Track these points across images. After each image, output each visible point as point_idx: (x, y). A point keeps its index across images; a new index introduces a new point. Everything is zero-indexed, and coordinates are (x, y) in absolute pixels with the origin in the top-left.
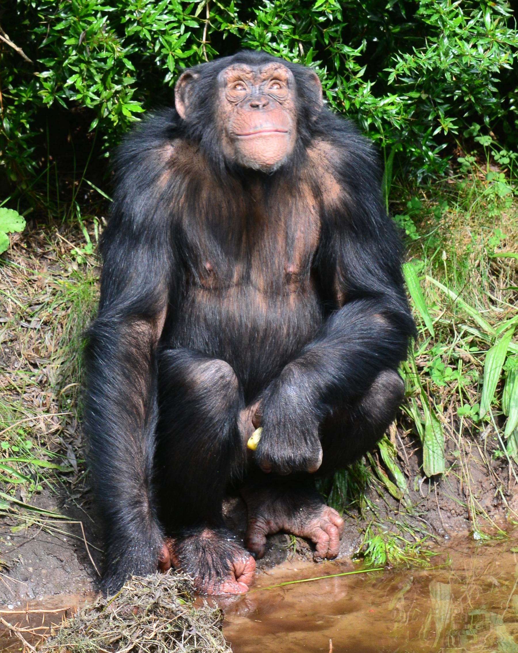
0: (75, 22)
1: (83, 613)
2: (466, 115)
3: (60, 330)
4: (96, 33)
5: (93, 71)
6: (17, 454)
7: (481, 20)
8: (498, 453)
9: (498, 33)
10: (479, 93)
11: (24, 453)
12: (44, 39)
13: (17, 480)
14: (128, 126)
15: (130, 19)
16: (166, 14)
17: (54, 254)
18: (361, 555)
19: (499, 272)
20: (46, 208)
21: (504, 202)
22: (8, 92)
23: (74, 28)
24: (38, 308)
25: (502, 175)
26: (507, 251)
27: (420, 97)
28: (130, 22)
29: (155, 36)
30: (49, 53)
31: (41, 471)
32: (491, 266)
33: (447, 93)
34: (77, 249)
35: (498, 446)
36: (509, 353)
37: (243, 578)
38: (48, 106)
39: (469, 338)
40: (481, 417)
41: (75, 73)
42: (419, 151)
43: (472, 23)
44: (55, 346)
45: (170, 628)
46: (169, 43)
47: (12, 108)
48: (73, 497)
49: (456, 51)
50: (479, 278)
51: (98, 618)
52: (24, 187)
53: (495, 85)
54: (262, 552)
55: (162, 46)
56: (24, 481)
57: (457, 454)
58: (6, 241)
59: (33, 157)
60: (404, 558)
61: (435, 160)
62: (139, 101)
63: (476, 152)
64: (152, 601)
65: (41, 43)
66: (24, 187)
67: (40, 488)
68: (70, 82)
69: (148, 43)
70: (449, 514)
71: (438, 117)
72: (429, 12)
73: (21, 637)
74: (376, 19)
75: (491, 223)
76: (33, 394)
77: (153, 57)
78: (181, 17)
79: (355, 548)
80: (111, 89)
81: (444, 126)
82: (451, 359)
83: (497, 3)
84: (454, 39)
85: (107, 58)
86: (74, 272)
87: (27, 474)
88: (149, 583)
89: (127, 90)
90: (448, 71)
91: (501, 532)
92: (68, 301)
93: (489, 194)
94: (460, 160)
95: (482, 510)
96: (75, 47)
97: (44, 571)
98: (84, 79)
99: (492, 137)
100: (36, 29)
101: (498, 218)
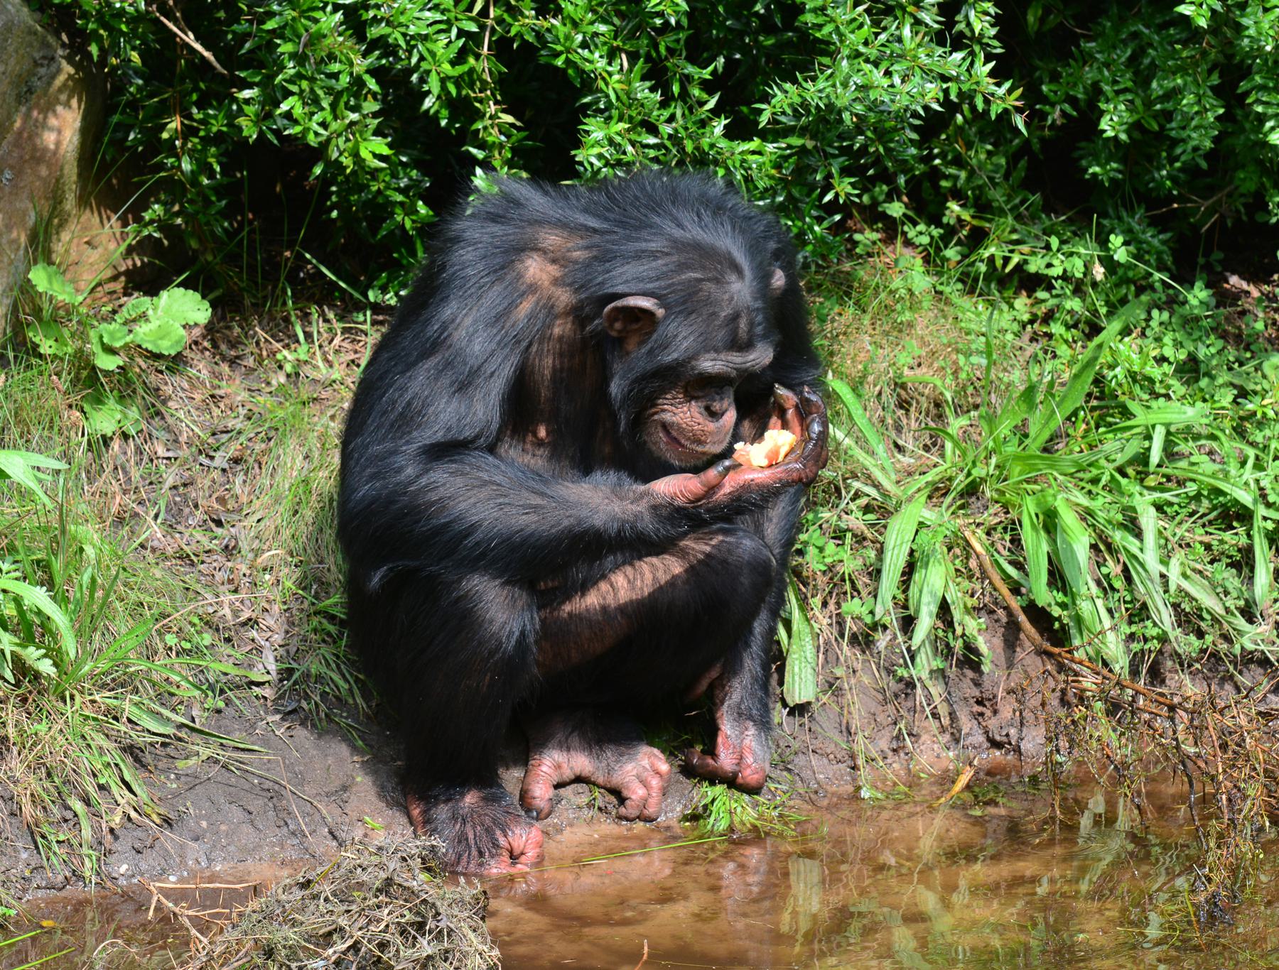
0: (294, 19)
1: (280, 891)
2: (871, 172)
3: (257, 470)
4: (325, 36)
5: (320, 93)
6: (188, 652)
7: (897, 33)
8: (901, 672)
9: (921, 53)
10: (892, 141)
11: (196, 651)
12: (246, 41)
13: (187, 692)
14: (367, 173)
15: (375, 16)
16: (429, 10)
17: (251, 359)
18: (694, 817)
19: (910, 404)
20: (241, 290)
21: (921, 302)
22: (189, 116)
23: (292, 27)
24: (225, 437)
25: (919, 261)
26: (924, 374)
27: (803, 146)
28: (376, 21)
29: (413, 43)
30: (252, 61)
31: (224, 679)
32: (899, 395)
33: (844, 140)
34: (285, 352)
35: (901, 661)
36: (921, 525)
37: (523, 858)
38: (251, 141)
39: (863, 501)
40: (877, 618)
41: (292, 94)
42: (800, 224)
43: (883, 37)
44: (249, 494)
45: (409, 916)
46: (433, 54)
47: (196, 140)
48: (270, 719)
49: (858, 79)
50: (880, 412)
51: (303, 899)
52: (210, 258)
53: (915, 128)
54: (546, 811)
55: (422, 58)
56: (197, 693)
57: (839, 672)
58: (182, 337)
59: (226, 214)
60: (758, 823)
61: (823, 238)
62: (385, 136)
63: (880, 225)
64: (383, 875)
65: (242, 46)
66: (210, 258)
67: (221, 704)
68: (284, 107)
69: (401, 52)
70: (825, 761)
71: (829, 176)
72: (820, 20)
73: (187, 923)
74: (738, 26)
75: (900, 331)
76: (215, 564)
77: (409, 71)
78: (452, 15)
79: (685, 806)
80: (343, 119)
81: (838, 189)
82: (835, 532)
83: (920, 8)
84: (856, 61)
85: (340, 72)
86: (281, 386)
87: (202, 684)
88: (380, 849)
89: (368, 121)
90: (846, 109)
91: (902, 788)
92: (270, 428)
93: (898, 289)
94: (857, 237)
95: (874, 754)
96: (293, 56)
97: (223, 827)
98: (305, 104)
99: (906, 205)
100: (235, 27)
101: (910, 325)
